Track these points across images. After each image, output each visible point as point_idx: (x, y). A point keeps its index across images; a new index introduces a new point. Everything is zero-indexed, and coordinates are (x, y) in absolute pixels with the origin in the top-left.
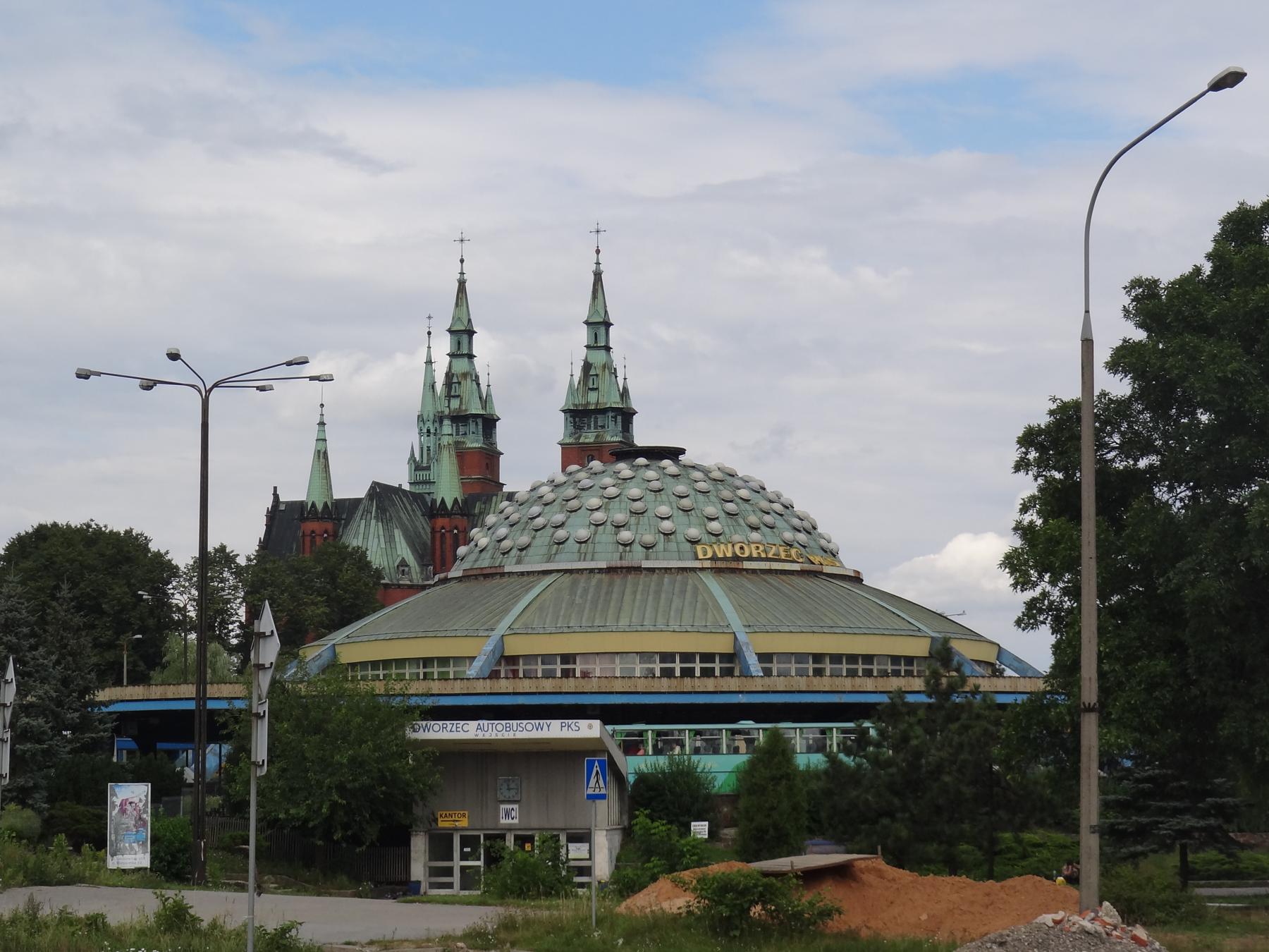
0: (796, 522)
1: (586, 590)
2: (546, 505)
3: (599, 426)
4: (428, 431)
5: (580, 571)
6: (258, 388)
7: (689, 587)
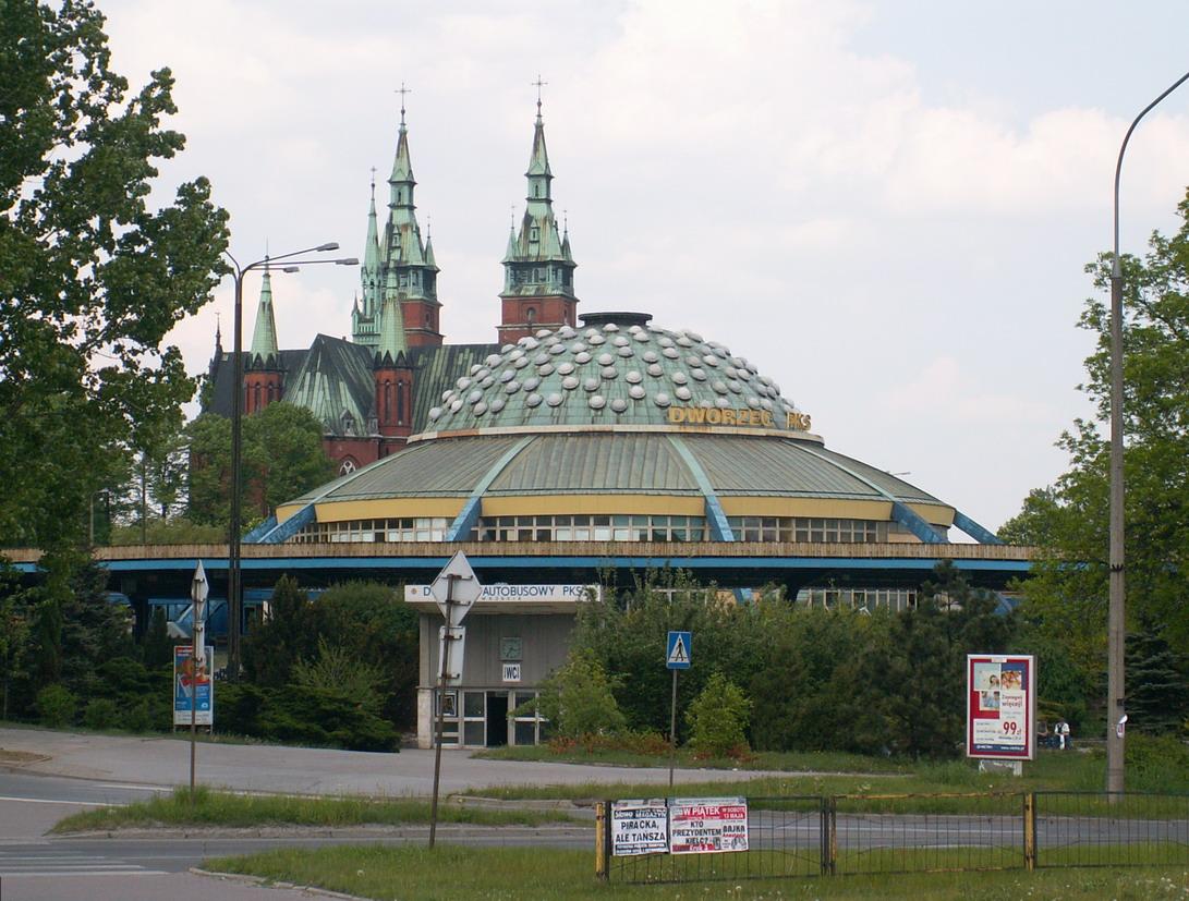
0: (761, 388)
1: (560, 454)
2: (519, 369)
3: (539, 285)
4: (372, 283)
5: (555, 434)
6: (285, 270)
7: (660, 452)
